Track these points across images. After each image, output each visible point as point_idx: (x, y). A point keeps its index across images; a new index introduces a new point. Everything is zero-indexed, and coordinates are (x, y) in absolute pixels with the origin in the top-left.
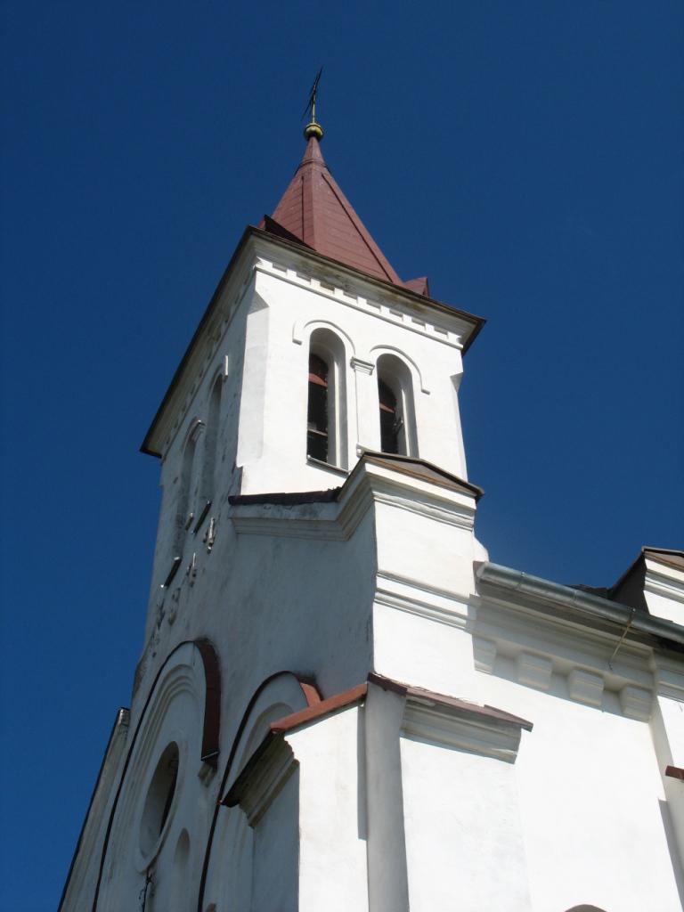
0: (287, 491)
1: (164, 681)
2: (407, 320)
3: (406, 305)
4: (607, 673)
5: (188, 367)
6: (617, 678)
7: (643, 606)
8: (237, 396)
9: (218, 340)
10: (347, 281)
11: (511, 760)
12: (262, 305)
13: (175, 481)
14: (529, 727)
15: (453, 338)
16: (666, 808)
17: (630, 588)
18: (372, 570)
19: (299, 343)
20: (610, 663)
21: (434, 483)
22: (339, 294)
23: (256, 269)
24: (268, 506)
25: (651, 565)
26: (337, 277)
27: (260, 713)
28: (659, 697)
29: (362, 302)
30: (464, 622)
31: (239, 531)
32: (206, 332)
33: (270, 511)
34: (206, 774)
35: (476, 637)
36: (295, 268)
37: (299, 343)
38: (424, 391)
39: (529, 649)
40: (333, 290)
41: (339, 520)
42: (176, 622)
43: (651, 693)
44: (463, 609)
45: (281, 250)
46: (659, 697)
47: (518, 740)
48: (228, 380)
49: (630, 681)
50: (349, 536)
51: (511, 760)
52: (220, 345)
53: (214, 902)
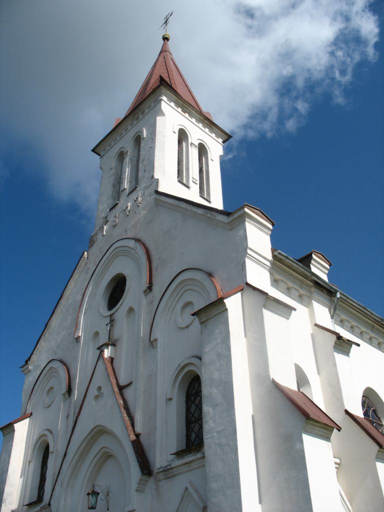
0: (195, 201)
1: (114, 250)
2: (207, 130)
3: (208, 125)
4: (300, 290)
5: (120, 126)
6: (303, 292)
7: (310, 268)
8: (152, 149)
9: (136, 120)
10: (190, 111)
11: (288, 319)
12: (163, 114)
13: (111, 169)
14: (295, 310)
15: (220, 140)
16: (312, 335)
17: (306, 260)
18: (246, 247)
19: (175, 133)
20: (301, 287)
21: (262, 218)
22: (187, 115)
23: (161, 99)
24: (182, 202)
25: (314, 256)
26: (187, 108)
27: (184, 278)
28: (313, 301)
29: (194, 120)
30: (268, 268)
31: (157, 203)
32: (132, 115)
33: (184, 205)
34: (147, 291)
35: (271, 274)
36: (174, 102)
37: (175, 133)
38: (211, 160)
39: (282, 279)
40: (185, 113)
41: (229, 223)
42: (116, 227)
43: (310, 298)
44: (268, 264)
45: (170, 93)
46: (313, 301)
47: (291, 313)
48: (145, 140)
49: (306, 294)
50: (231, 229)
51: (288, 319)
52: (137, 123)
53: (157, 338)
